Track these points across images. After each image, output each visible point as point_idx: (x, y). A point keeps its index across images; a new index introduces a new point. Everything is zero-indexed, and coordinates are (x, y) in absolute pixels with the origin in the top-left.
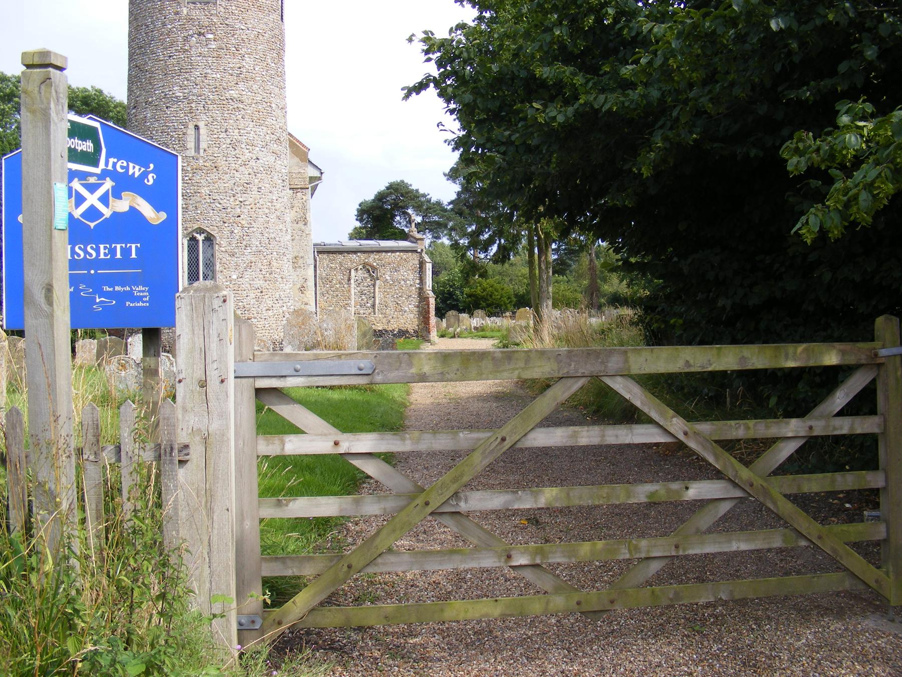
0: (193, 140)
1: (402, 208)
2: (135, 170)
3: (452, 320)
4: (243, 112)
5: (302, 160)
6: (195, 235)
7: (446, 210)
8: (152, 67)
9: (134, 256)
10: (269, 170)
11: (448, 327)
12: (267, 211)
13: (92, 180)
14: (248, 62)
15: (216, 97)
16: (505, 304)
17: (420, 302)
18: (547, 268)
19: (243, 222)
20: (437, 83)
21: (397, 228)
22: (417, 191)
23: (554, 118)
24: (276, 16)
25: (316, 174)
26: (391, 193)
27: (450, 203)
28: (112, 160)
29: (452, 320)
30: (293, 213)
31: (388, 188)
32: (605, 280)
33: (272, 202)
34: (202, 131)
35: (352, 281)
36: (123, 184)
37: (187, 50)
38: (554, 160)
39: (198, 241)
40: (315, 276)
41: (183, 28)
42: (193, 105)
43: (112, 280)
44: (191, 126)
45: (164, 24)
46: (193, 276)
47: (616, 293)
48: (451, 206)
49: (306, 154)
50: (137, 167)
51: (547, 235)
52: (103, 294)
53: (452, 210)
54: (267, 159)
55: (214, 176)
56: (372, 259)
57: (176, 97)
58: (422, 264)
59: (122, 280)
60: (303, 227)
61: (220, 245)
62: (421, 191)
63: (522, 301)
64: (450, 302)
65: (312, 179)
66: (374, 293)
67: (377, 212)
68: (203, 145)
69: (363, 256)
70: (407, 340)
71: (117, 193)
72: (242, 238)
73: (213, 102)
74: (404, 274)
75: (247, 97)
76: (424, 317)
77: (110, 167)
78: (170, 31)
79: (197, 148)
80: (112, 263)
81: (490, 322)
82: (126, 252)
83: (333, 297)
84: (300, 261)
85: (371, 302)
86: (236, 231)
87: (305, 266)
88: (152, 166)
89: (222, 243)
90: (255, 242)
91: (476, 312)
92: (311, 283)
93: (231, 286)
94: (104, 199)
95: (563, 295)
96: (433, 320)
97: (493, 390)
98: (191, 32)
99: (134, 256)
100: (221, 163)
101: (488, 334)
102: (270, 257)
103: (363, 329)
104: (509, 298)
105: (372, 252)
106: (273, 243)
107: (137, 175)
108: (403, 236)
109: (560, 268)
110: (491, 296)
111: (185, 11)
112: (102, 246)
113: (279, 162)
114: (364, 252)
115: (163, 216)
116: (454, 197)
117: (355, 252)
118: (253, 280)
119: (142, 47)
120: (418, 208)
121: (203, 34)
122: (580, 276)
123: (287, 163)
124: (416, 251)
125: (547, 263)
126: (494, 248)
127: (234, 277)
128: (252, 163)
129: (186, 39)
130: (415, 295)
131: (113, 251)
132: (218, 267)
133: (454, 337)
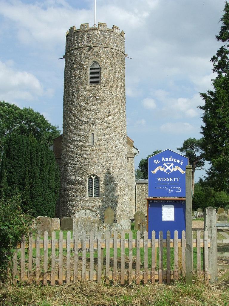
2: (178, 161)
9: (178, 181)
10: (120, 151)
13: (168, 163)
15: (100, 122)
25: (136, 151)
28: (173, 159)
36: (176, 164)
39: (93, 179)
41: (87, 94)
42: (91, 125)
43: (173, 186)
44: (90, 133)
45: (79, 93)
49: (132, 144)
50: (179, 161)
52: (171, 189)
54: (120, 147)
55: (99, 154)
60: (131, 174)
68: (95, 141)
73: (99, 124)
77: (172, 161)
79: (93, 143)
80: (173, 182)
82: (176, 180)
83: (142, 202)
84: (130, 187)
86: (108, 176)
88: (182, 160)
92: (134, 197)
94: (171, 168)
98: (90, 96)
99: (178, 181)
100: (102, 148)
107: (179, 162)
112: (171, 178)
113: (124, 148)
115: (185, 172)
123: (126, 148)
127: (107, 194)
129: (88, 99)
131: (173, 180)
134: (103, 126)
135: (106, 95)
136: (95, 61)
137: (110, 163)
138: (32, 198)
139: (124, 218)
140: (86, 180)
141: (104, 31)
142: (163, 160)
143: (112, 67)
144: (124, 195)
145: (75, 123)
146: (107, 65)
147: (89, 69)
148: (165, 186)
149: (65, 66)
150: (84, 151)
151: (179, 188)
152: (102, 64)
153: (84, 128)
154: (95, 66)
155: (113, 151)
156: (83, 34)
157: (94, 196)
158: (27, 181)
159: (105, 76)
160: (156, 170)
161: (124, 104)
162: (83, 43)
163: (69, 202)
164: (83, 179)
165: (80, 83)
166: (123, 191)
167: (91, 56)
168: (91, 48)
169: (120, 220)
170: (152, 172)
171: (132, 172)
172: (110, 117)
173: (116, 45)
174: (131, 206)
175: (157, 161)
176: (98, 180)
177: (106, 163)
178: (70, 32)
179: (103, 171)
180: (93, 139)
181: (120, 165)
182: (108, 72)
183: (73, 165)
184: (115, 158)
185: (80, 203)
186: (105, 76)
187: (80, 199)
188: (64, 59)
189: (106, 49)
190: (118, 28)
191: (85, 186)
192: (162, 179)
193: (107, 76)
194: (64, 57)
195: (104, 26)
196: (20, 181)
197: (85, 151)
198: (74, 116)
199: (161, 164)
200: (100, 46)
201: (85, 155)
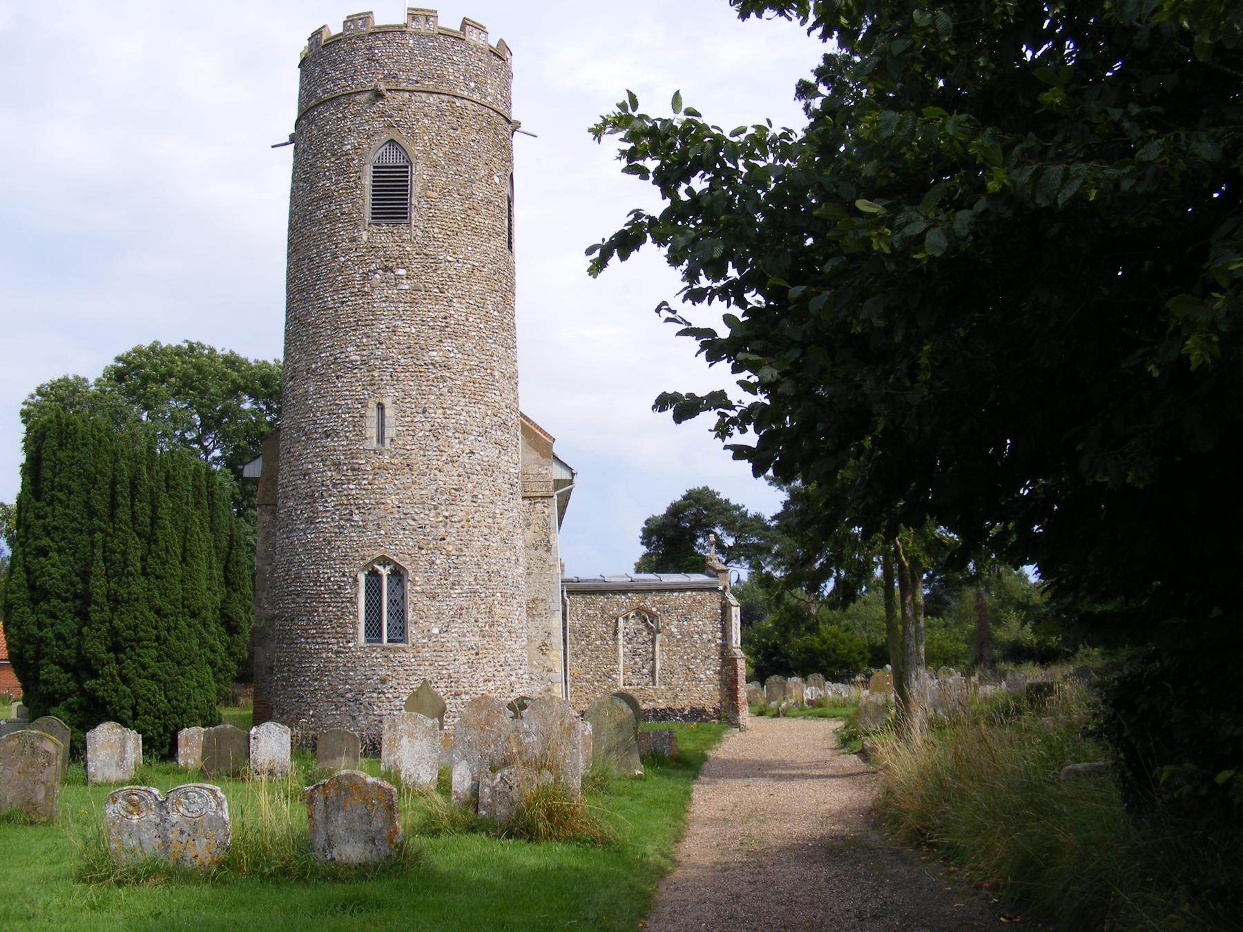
0: (374, 424)
3: (775, 690)
4: (449, 383)
6: (377, 567)
7: (768, 528)
10: (490, 469)
11: (769, 700)
12: (486, 531)
14: (458, 310)
16: (856, 662)
17: (722, 667)
18: (915, 615)
19: (450, 548)
20: (660, 229)
22: (727, 501)
23: (919, 240)
24: (501, 242)
25: (565, 475)
26: (690, 505)
27: (774, 518)
29: (775, 690)
30: (529, 534)
31: (685, 498)
32: (998, 622)
33: (494, 517)
34: (388, 412)
35: (620, 636)
37: (367, 293)
38: (924, 361)
39: (381, 576)
40: (564, 628)
41: (362, 261)
42: (376, 374)
44: (372, 405)
46: (373, 631)
47: (1015, 642)
51: (914, 561)
53: (777, 527)
54: (487, 453)
55: (405, 479)
56: (650, 602)
58: (725, 608)
60: (545, 555)
61: (414, 583)
62: (733, 502)
63: (878, 657)
64: (772, 662)
65: (559, 483)
66: (653, 652)
67: (671, 533)
68: (390, 432)
69: (636, 598)
70: (703, 725)
72: (446, 574)
74: (701, 625)
75: (456, 359)
76: (729, 689)
79: (381, 439)
81: (833, 691)
83: (591, 659)
84: (541, 606)
85: (648, 666)
86: (438, 562)
87: (549, 612)
89: (417, 582)
90: (468, 578)
91: (810, 677)
92: (557, 638)
93: (430, 644)
95: (940, 647)
96: (744, 690)
97: (826, 830)
98: (373, 267)
100: (417, 459)
101: (828, 710)
102: (490, 600)
103: (618, 718)
104: (861, 653)
105: (650, 591)
106: (496, 580)
108: (700, 565)
109: (935, 607)
110: (834, 651)
111: (365, 236)
113: (506, 458)
114: (692, 590)
116: (779, 509)
118: (464, 636)
119: (303, 290)
120: (729, 527)
121: (391, 270)
122: (961, 618)
124: (716, 589)
125: (916, 607)
126: (830, 585)
127: (435, 631)
128: (464, 459)
129: (366, 277)
130: (715, 656)
132: (411, 616)
133: (777, 715)
134: (419, 377)
135: (433, 263)
137: (446, 514)
138: (116, 648)
139: (411, 736)
140: (356, 580)
143: (456, 160)
146: (438, 155)
147: (369, 169)
150: (350, 473)
152: (416, 150)
153: (349, 386)
154: (392, 159)
155: (461, 470)
157: (389, 641)
158: (99, 586)
159: (430, 193)
161: (504, 297)
162: (353, 80)
163: (300, 663)
164: (344, 575)
166: (504, 621)
168: (379, 95)
169: (395, 742)
172: (447, 344)
173: (472, 85)
174: (544, 674)
177: (433, 513)
179: (422, 545)
180: (383, 425)
181: (490, 520)
184: (468, 497)
185: (337, 668)
186: (430, 193)
187: (337, 652)
189: (433, 99)
190: (481, 29)
193: (435, 194)
194: (293, 139)
195: (427, 20)
196: (73, 584)
197: (353, 470)
200: (410, 87)
201: (351, 486)
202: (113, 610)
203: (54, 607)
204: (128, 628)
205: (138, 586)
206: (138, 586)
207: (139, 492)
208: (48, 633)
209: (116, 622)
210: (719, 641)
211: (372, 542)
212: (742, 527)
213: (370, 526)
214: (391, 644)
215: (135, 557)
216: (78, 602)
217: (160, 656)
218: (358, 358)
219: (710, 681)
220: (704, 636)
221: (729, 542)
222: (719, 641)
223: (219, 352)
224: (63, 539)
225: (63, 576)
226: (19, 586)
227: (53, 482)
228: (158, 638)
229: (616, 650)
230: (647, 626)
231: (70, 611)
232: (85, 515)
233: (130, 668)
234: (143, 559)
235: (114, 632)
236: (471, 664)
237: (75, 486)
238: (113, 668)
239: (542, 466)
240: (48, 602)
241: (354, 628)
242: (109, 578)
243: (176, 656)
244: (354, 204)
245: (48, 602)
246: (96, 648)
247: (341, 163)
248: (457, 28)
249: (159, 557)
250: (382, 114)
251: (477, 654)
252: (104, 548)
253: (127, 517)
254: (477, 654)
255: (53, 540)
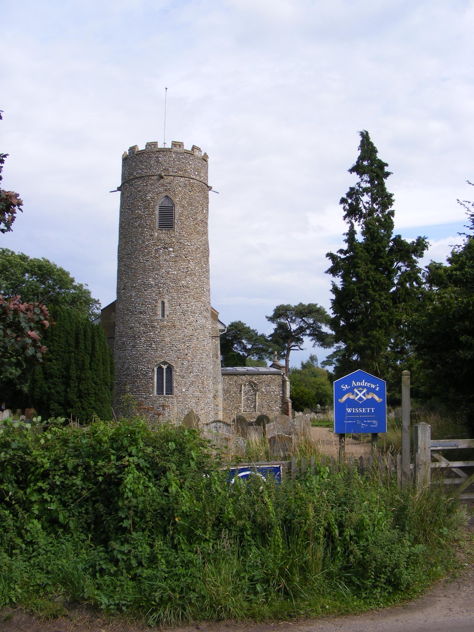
0: (161, 310)
1: (239, 339)
2: (373, 386)
5: (214, 320)
7: (267, 341)
8: (136, 266)
13: (360, 389)
14: (192, 265)
15: (174, 285)
16: (311, 403)
17: (282, 405)
19: (189, 358)
21: (235, 352)
22: (249, 328)
26: (232, 329)
27: (270, 336)
33: (204, 346)
35: (242, 392)
36: (370, 390)
39: (163, 369)
41: (155, 245)
43: (366, 419)
44: (160, 302)
45: (143, 242)
46: (160, 391)
48: (270, 338)
53: (271, 340)
55: (173, 331)
56: (254, 379)
57: (151, 284)
58: (284, 382)
59: (370, 419)
60: (216, 360)
61: (176, 372)
62: (251, 328)
66: (255, 399)
68: (167, 313)
69: (249, 377)
71: (368, 393)
72: (188, 368)
78: (147, 246)
79: (163, 315)
80: (366, 414)
82: (370, 410)
83: (231, 401)
86: (185, 363)
94: (364, 395)
105: (255, 375)
110: (302, 398)
111: (156, 234)
113: (208, 323)
115: (381, 400)
116: (272, 332)
117: (244, 374)
118: (194, 392)
119: (129, 254)
120: (249, 340)
124: (280, 374)
127: (184, 390)
129: (157, 251)
131: (367, 410)
132: (175, 384)
134: (178, 291)
136: (167, 197)
138: (80, 397)
140: (153, 370)
141: (180, 153)
142: (354, 385)
143: (191, 204)
144: (208, 392)
145: (136, 286)
146: (184, 202)
147: (157, 208)
148: (355, 419)
149: (121, 203)
150: (151, 328)
151: (374, 422)
152: (177, 200)
154: (167, 204)
155: (193, 328)
156: (150, 157)
157: (166, 394)
158: (74, 373)
159: (182, 218)
160: (345, 398)
164: (148, 368)
165: (145, 227)
167: (161, 190)
168: (161, 177)
170: (339, 400)
171: (217, 358)
172: (188, 279)
173: (196, 173)
175: (346, 386)
176: (171, 371)
177: (183, 345)
178: (130, 153)
179: (179, 357)
181: (203, 347)
182: (186, 213)
183: (134, 347)
184: (195, 338)
186: (182, 218)
187: (146, 398)
188: (119, 193)
190: (199, 149)
191: (152, 378)
192: (352, 410)
193: (183, 218)
194: (119, 189)
196: (62, 372)
197: (152, 327)
198: (135, 276)
199: (351, 390)
200: (174, 174)
201: (151, 334)
202: (79, 383)
203: (55, 381)
204: (86, 390)
205: (89, 373)
206: (89, 373)
207: (87, 338)
208: (53, 391)
209: (81, 387)
210: (281, 395)
211: (161, 355)
212: (255, 340)
213: (159, 349)
214: (167, 395)
215: (87, 361)
216: (64, 379)
217: (96, 400)
218: (154, 283)
219: (277, 411)
220: (275, 393)
221: (249, 346)
222: (281, 395)
223: (17, 254)
224: (58, 355)
225: (58, 369)
226: (40, 373)
227: (52, 333)
228: (95, 393)
229: (241, 398)
230: (253, 388)
231: (61, 383)
232: (67, 346)
233: (86, 405)
234: (90, 364)
235: (79, 390)
236: (196, 403)
237: (62, 335)
238: (79, 404)
239: (214, 324)
240: (52, 379)
241: (153, 389)
242: (77, 370)
243: (101, 400)
244: (152, 221)
245: (52, 379)
246: (73, 396)
247: (146, 204)
248: (190, 150)
249: (96, 362)
250: (163, 185)
251: (198, 399)
252: (75, 358)
253: (83, 347)
254: (198, 399)
255: (53, 355)
